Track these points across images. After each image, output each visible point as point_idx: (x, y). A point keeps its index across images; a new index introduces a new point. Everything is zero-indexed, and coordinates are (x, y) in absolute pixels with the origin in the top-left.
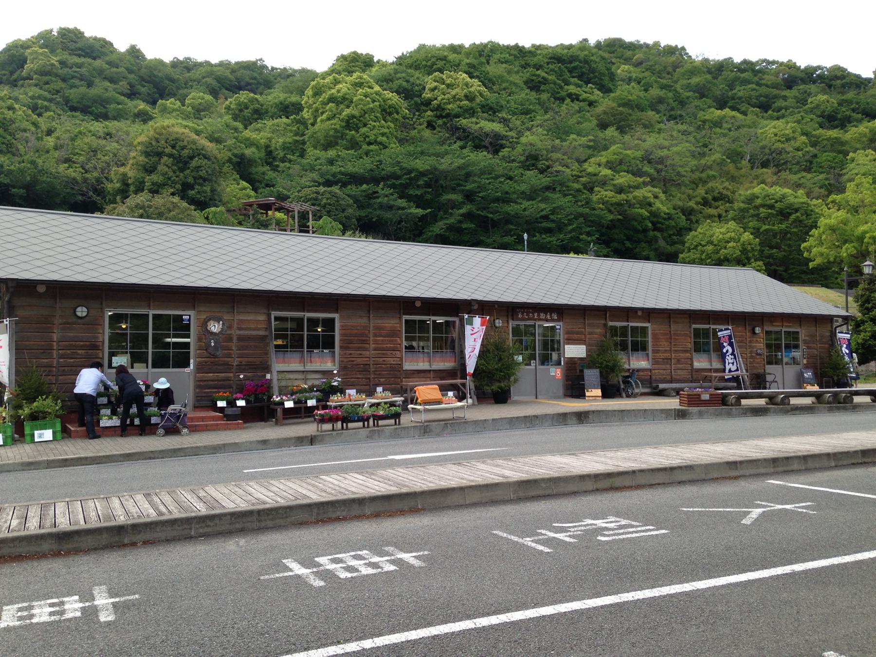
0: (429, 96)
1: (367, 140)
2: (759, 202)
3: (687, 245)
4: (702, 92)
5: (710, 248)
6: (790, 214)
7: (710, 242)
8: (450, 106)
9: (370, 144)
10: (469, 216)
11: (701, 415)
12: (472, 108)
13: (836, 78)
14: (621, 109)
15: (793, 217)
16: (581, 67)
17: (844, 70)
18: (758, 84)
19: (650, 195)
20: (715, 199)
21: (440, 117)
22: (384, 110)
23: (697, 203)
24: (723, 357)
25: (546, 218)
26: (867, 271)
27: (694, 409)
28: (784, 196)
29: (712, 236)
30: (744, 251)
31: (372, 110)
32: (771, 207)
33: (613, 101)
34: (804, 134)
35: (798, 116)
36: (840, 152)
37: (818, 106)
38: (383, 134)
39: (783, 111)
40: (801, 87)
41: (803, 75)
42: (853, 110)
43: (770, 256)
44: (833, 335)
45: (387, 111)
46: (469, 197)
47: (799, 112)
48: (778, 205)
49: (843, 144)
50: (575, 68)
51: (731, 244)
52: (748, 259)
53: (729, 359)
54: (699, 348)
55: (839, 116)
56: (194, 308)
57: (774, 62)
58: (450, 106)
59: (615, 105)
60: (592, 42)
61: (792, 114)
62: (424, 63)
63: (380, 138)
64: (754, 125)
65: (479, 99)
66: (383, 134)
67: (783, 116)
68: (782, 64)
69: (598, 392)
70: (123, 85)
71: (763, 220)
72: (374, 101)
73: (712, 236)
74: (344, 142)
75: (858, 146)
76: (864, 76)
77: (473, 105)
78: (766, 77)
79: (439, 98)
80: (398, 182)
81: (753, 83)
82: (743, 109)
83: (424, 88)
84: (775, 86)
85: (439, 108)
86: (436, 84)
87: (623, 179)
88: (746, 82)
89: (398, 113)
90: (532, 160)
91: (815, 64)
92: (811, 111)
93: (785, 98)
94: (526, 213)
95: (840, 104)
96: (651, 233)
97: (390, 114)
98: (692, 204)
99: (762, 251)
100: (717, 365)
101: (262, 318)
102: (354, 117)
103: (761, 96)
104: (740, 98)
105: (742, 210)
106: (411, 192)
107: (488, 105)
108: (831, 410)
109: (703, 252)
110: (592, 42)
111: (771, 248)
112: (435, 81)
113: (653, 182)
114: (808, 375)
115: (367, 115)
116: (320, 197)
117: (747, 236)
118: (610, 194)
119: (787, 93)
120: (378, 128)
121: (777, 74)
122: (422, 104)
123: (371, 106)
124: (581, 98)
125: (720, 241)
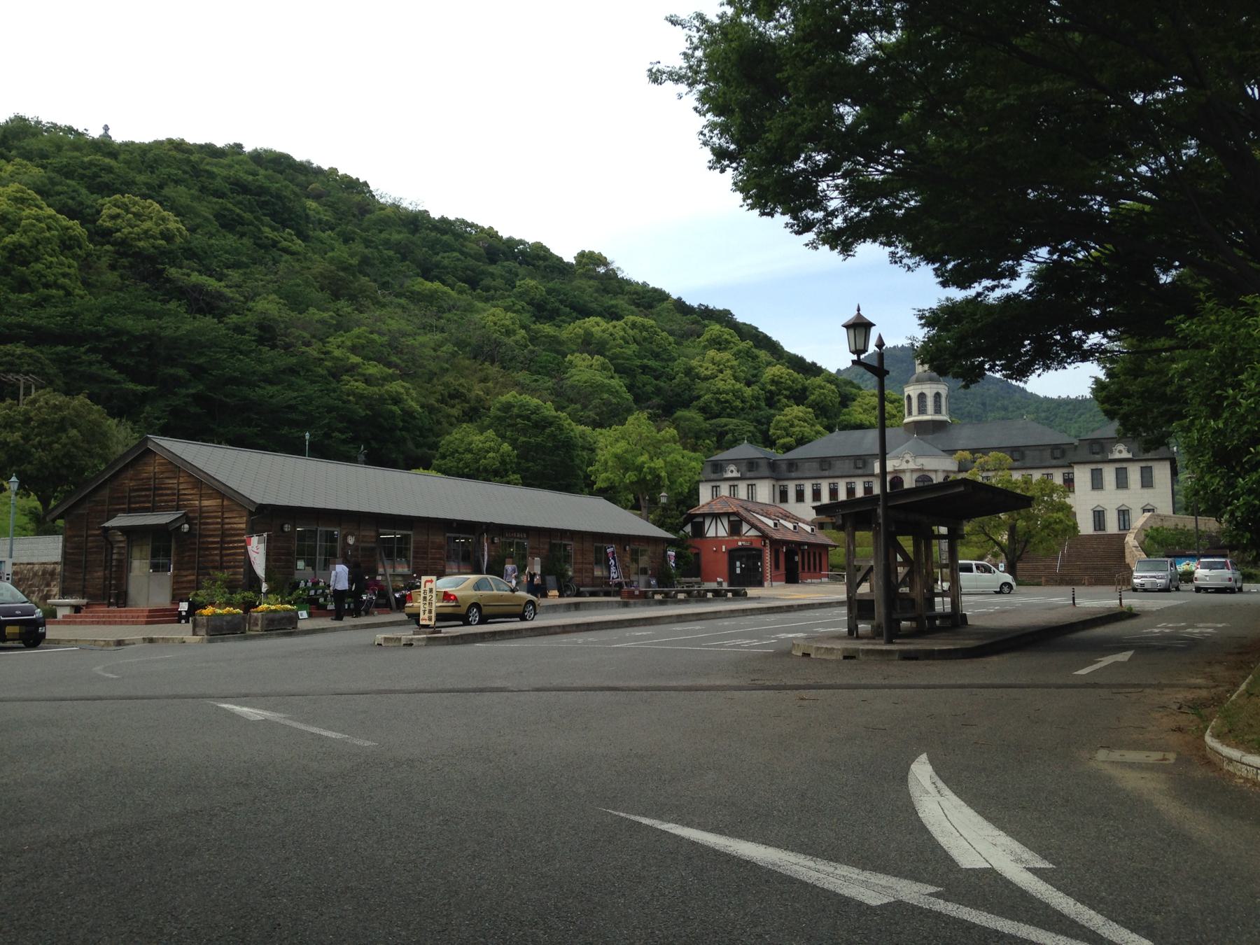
0: (108, 224)
1: (44, 280)
2: (516, 411)
3: (441, 450)
4: (404, 253)
5: (469, 456)
6: (544, 428)
7: (470, 451)
8: (141, 244)
9: (47, 286)
10: (198, 398)
11: (635, 604)
12: (171, 252)
13: (538, 257)
14: (341, 274)
15: (548, 431)
16: (274, 204)
17: (547, 250)
18: (462, 253)
19: (402, 390)
20: (451, 396)
21: (125, 255)
22: (63, 242)
23: (438, 401)
24: (609, 567)
25: (292, 408)
26: (663, 500)
27: (632, 601)
28: (538, 408)
29: (470, 444)
30: (503, 462)
31: (48, 241)
32: (528, 418)
33: (330, 263)
34: (523, 327)
35: (509, 301)
36: (557, 352)
37: (526, 292)
38: (65, 275)
39: (492, 292)
40: (506, 263)
41: (504, 248)
42: (561, 302)
43: (528, 469)
44: (665, 552)
45: (67, 244)
46: (198, 372)
47: (509, 296)
48: (533, 417)
49: (561, 343)
50: (266, 203)
51: (491, 455)
52: (506, 471)
53: (613, 569)
54: (598, 562)
55: (548, 307)
56: (340, 525)
57: (472, 225)
58: (141, 244)
59: (333, 268)
60: (248, 148)
61: (503, 297)
62: (81, 171)
63: (62, 281)
64: (469, 309)
65: (178, 240)
66: (65, 275)
67: (493, 298)
68: (482, 229)
69: (556, 593)
70: (438, 396)
71: (524, 431)
72: (49, 229)
73: (470, 444)
74: (9, 280)
75: (575, 348)
76: (566, 260)
77: (173, 247)
78: (467, 243)
79: (125, 231)
80: (103, 345)
81: (454, 250)
82: (450, 281)
83: (98, 212)
84: (477, 257)
85: (123, 242)
86: (118, 211)
87: (373, 369)
88: (448, 248)
89: (81, 249)
90: (267, 333)
91: (517, 238)
92: (520, 296)
93: (492, 275)
94: (274, 401)
95: (549, 292)
96: (398, 432)
97: (70, 248)
98: (432, 401)
99: (518, 464)
100: (605, 573)
101: (373, 534)
102: (21, 246)
103: (467, 268)
104: (445, 268)
105: (498, 418)
106: (119, 360)
107: (190, 249)
108: (697, 602)
109: (461, 460)
110: (248, 148)
111: (527, 461)
112: (115, 205)
113: (405, 376)
114: (653, 582)
115: (40, 247)
116: (17, 361)
117: (506, 447)
118: (361, 385)
119: (491, 269)
120: (61, 266)
121: (476, 241)
122: (97, 233)
123: (47, 234)
124: (279, 245)
125: (480, 450)
